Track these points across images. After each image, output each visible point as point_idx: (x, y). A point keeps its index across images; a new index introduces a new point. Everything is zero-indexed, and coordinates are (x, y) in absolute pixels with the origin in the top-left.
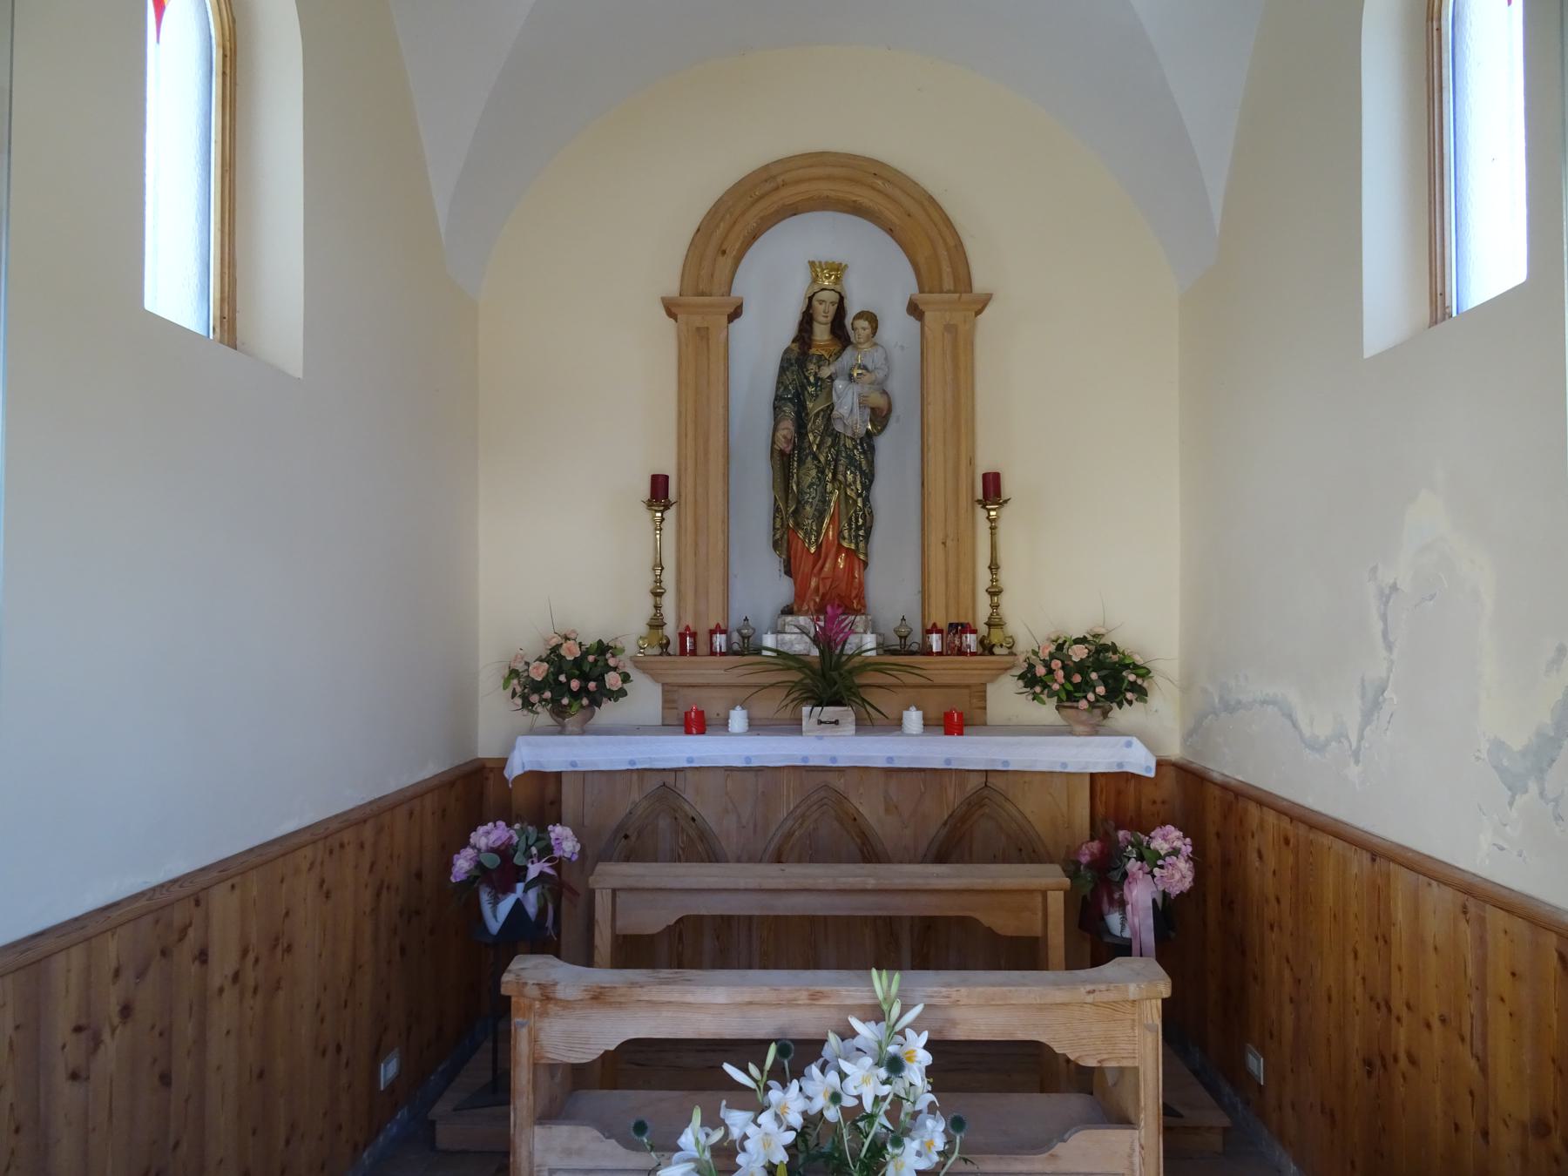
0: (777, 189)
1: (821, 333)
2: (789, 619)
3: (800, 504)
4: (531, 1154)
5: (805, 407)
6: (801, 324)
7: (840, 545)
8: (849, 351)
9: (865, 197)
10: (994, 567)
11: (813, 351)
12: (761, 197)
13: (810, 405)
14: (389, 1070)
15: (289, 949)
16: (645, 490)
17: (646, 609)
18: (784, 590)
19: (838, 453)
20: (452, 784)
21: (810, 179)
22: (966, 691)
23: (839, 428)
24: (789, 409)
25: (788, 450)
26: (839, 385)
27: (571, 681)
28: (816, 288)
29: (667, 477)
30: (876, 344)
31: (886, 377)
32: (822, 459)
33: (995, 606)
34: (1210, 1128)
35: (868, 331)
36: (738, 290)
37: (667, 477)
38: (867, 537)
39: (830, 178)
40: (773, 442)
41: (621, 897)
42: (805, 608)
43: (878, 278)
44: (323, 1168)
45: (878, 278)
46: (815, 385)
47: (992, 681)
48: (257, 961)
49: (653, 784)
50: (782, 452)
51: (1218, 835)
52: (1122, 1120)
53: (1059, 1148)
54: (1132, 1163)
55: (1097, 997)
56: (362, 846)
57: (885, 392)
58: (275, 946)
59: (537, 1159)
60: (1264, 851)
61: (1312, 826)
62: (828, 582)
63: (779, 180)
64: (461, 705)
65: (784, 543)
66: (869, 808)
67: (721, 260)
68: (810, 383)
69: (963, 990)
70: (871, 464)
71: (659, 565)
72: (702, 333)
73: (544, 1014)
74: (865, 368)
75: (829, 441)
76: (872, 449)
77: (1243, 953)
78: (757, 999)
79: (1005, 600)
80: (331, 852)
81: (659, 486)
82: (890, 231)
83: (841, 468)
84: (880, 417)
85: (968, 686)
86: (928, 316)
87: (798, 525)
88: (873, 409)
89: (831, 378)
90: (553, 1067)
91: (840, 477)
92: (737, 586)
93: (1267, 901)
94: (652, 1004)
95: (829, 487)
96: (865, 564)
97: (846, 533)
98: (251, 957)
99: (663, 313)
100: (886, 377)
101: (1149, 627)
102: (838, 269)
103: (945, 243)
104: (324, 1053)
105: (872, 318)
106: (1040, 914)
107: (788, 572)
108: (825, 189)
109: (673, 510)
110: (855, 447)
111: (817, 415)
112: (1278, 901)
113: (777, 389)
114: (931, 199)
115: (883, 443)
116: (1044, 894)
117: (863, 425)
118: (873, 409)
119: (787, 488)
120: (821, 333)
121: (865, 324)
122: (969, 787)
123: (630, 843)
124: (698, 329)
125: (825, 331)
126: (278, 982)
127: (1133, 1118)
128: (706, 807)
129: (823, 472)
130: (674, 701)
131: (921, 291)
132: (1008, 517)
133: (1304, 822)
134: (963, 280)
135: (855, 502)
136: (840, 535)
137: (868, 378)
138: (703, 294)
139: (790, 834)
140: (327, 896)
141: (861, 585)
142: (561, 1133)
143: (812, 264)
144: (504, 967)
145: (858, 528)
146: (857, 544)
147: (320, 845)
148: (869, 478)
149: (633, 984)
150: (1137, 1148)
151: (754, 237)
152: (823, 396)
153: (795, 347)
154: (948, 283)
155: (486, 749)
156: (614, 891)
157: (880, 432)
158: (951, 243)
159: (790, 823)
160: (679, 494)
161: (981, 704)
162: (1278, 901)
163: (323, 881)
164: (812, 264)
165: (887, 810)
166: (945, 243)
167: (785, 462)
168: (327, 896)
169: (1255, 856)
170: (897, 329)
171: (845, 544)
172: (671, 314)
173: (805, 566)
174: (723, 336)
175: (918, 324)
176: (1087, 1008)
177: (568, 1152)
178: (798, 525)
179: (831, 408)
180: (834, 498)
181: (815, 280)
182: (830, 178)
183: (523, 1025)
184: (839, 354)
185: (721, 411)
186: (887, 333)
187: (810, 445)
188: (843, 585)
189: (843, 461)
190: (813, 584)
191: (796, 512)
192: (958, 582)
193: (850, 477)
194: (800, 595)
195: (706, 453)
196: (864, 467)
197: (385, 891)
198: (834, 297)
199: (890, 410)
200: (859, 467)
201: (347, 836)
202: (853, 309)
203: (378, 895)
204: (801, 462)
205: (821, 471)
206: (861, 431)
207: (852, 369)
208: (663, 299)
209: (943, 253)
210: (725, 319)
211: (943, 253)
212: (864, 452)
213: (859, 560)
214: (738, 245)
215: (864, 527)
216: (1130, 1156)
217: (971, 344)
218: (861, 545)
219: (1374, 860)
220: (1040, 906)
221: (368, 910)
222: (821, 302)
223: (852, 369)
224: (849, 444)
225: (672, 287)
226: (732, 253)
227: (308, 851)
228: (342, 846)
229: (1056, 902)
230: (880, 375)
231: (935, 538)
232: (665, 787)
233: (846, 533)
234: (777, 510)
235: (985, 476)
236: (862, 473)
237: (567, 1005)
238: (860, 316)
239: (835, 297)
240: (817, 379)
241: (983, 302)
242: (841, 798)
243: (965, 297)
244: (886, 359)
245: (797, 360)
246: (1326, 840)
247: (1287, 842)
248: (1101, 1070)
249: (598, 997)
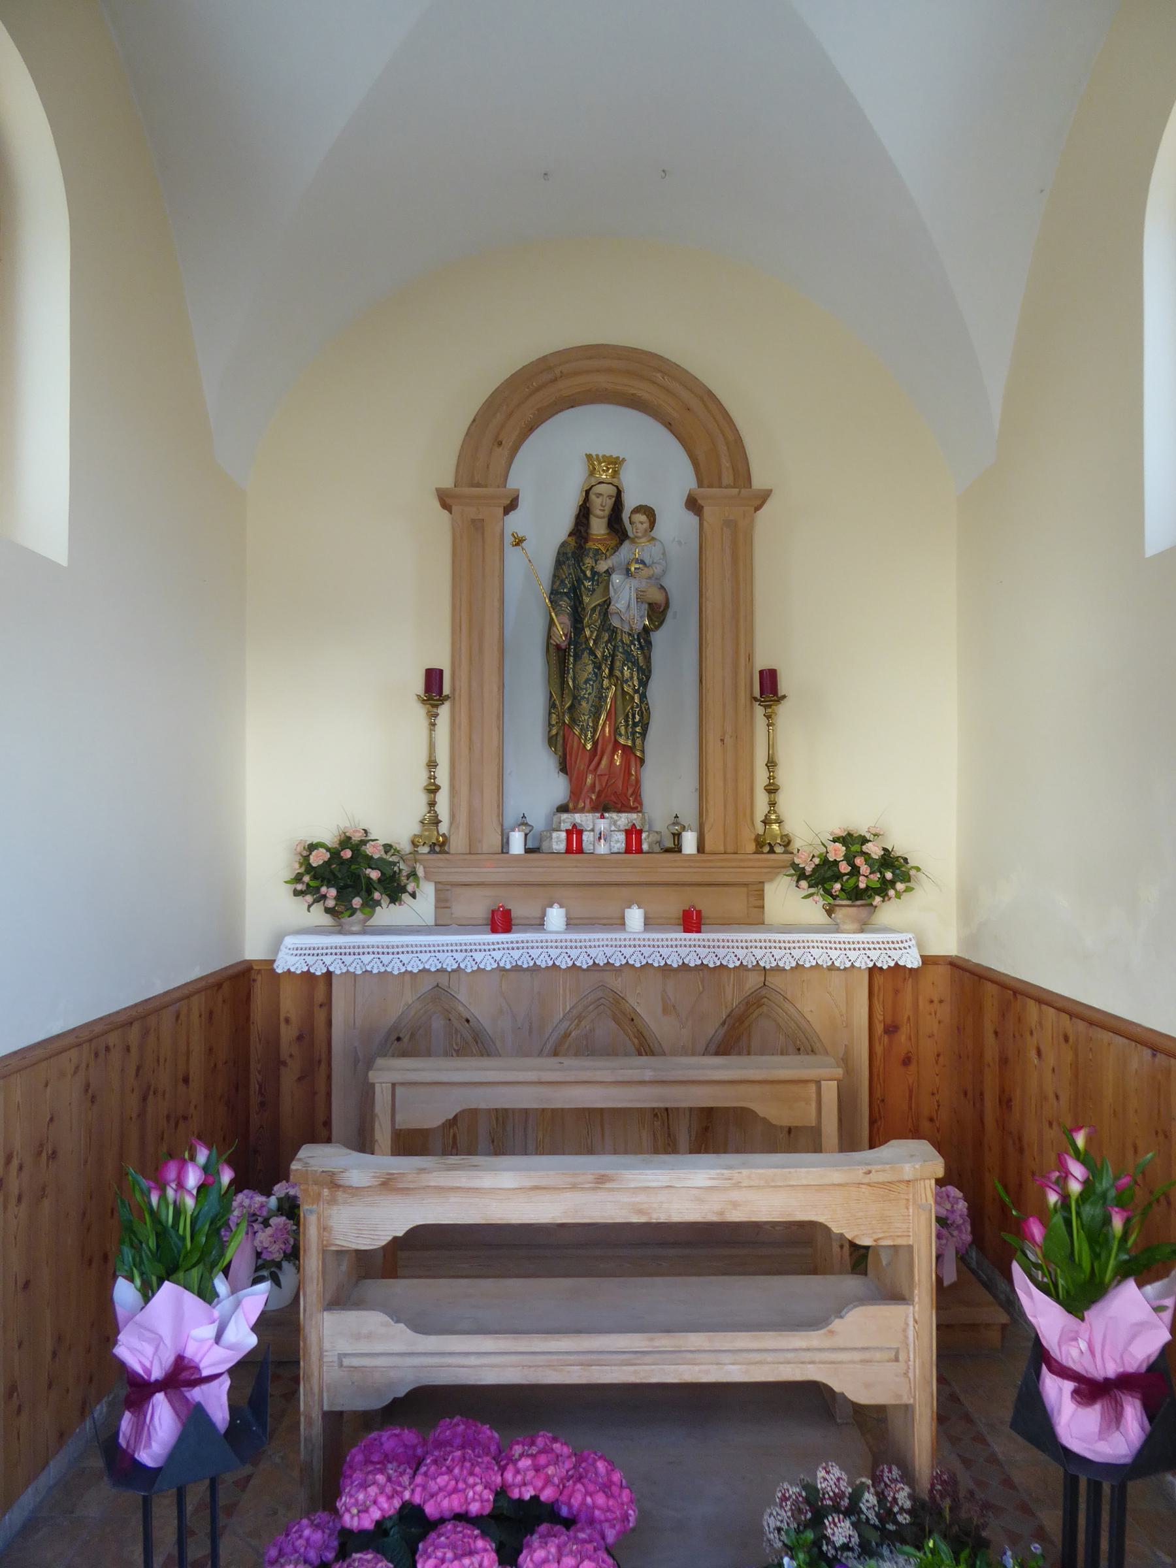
0: (555, 380)
1: (598, 527)
2: (564, 816)
4: (320, 1340)
5: (581, 602)
6: (578, 517)
7: (616, 742)
8: (627, 545)
9: (643, 390)
10: (771, 764)
11: (590, 545)
12: (538, 390)
13: (586, 600)
15: (54, 1155)
16: (419, 686)
17: (418, 805)
19: (615, 647)
20: (219, 985)
21: (588, 372)
22: (745, 889)
23: (615, 622)
24: (565, 603)
25: (564, 645)
26: (616, 579)
27: (346, 877)
29: (441, 671)
30: (653, 539)
31: (664, 572)
33: (773, 804)
34: (988, 1326)
35: (646, 525)
36: (512, 484)
37: (441, 671)
38: (644, 734)
39: (609, 370)
40: (549, 637)
41: (399, 1090)
42: (581, 805)
43: (656, 473)
44: (91, 1381)
45: (656, 473)
46: (592, 579)
47: (771, 880)
48: (21, 1168)
49: (426, 985)
50: (558, 647)
51: (996, 1033)
52: (896, 1296)
53: (837, 1324)
54: (906, 1337)
55: (874, 1177)
56: (128, 1049)
57: (662, 587)
58: (39, 1153)
59: (327, 1345)
60: (1042, 1048)
61: (1091, 1023)
63: (557, 371)
64: (226, 903)
65: (561, 743)
66: (645, 1004)
68: (586, 578)
69: (745, 1172)
70: (648, 659)
71: (432, 764)
72: (478, 526)
73: (333, 1201)
74: (643, 562)
75: (606, 636)
77: (1021, 1150)
78: (543, 1183)
79: (782, 798)
80: (96, 1055)
81: (433, 679)
82: (669, 425)
83: (618, 664)
84: (658, 612)
85: (746, 885)
86: (707, 510)
87: (574, 720)
88: (650, 604)
89: (608, 573)
90: (340, 1253)
92: (512, 784)
93: (1046, 1098)
94: (440, 1190)
95: (606, 683)
96: (642, 761)
97: (623, 730)
98: (15, 1163)
99: (437, 505)
100: (664, 572)
101: (919, 819)
102: (615, 463)
104: (90, 1262)
105: (649, 513)
106: (814, 1104)
107: (564, 768)
108: (602, 381)
110: (632, 643)
112: (1057, 1097)
113: (553, 583)
114: (710, 394)
115: (659, 638)
116: (818, 1083)
117: (639, 619)
118: (650, 604)
120: (598, 527)
121: (643, 518)
122: (748, 986)
123: (403, 1041)
124: (473, 521)
125: (603, 524)
126: (44, 1189)
127: (906, 1293)
128: (480, 1007)
129: (599, 668)
130: (447, 901)
131: (700, 484)
132: (783, 709)
133: (1083, 1019)
134: (743, 475)
136: (616, 731)
137: (645, 572)
138: (478, 485)
139: (567, 1035)
140: (93, 1100)
141: (638, 782)
142: (351, 1318)
143: (589, 457)
144: (292, 1156)
145: (635, 725)
146: (634, 741)
147: (86, 1046)
148: (645, 675)
149: (422, 1170)
150: (911, 1322)
151: (531, 429)
153: (572, 541)
154: (727, 478)
155: (253, 951)
156: (394, 1085)
157: (657, 628)
159: (566, 1024)
160: (453, 689)
161: (758, 903)
162: (1057, 1097)
163: (88, 1086)
164: (589, 457)
165: (665, 1011)
167: (560, 658)
168: (93, 1100)
169: (1033, 1054)
171: (622, 741)
172: (446, 506)
173: (581, 764)
176: (864, 1188)
177: (357, 1337)
178: (574, 720)
179: (608, 603)
180: (611, 694)
181: (592, 473)
182: (609, 370)
183: (311, 1212)
184: (616, 549)
185: (496, 604)
187: (587, 640)
189: (620, 656)
190: (589, 781)
191: (570, 708)
193: (627, 673)
194: (576, 792)
197: (151, 1097)
198: (612, 490)
199: (667, 605)
200: (635, 663)
201: (113, 1039)
202: (630, 501)
203: (145, 1099)
204: (577, 657)
206: (638, 627)
207: (629, 564)
208: (438, 490)
209: (722, 448)
210: (501, 510)
211: (722, 448)
213: (634, 757)
215: (642, 724)
216: (905, 1330)
218: (638, 742)
219: (1154, 1055)
220: (814, 1096)
221: (134, 1116)
222: (599, 495)
223: (629, 564)
224: (626, 639)
225: (447, 481)
226: (508, 444)
227: (73, 1053)
228: (107, 1049)
229: (830, 1091)
230: (657, 570)
232: (439, 988)
233: (623, 730)
234: (553, 706)
235: (761, 672)
236: (640, 669)
237: (355, 1191)
238: (638, 510)
239: (613, 491)
241: (763, 497)
242: (618, 999)
243: (743, 491)
244: (664, 553)
246: (1107, 1036)
247: (1066, 1039)
248: (876, 1249)
249: (388, 1185)
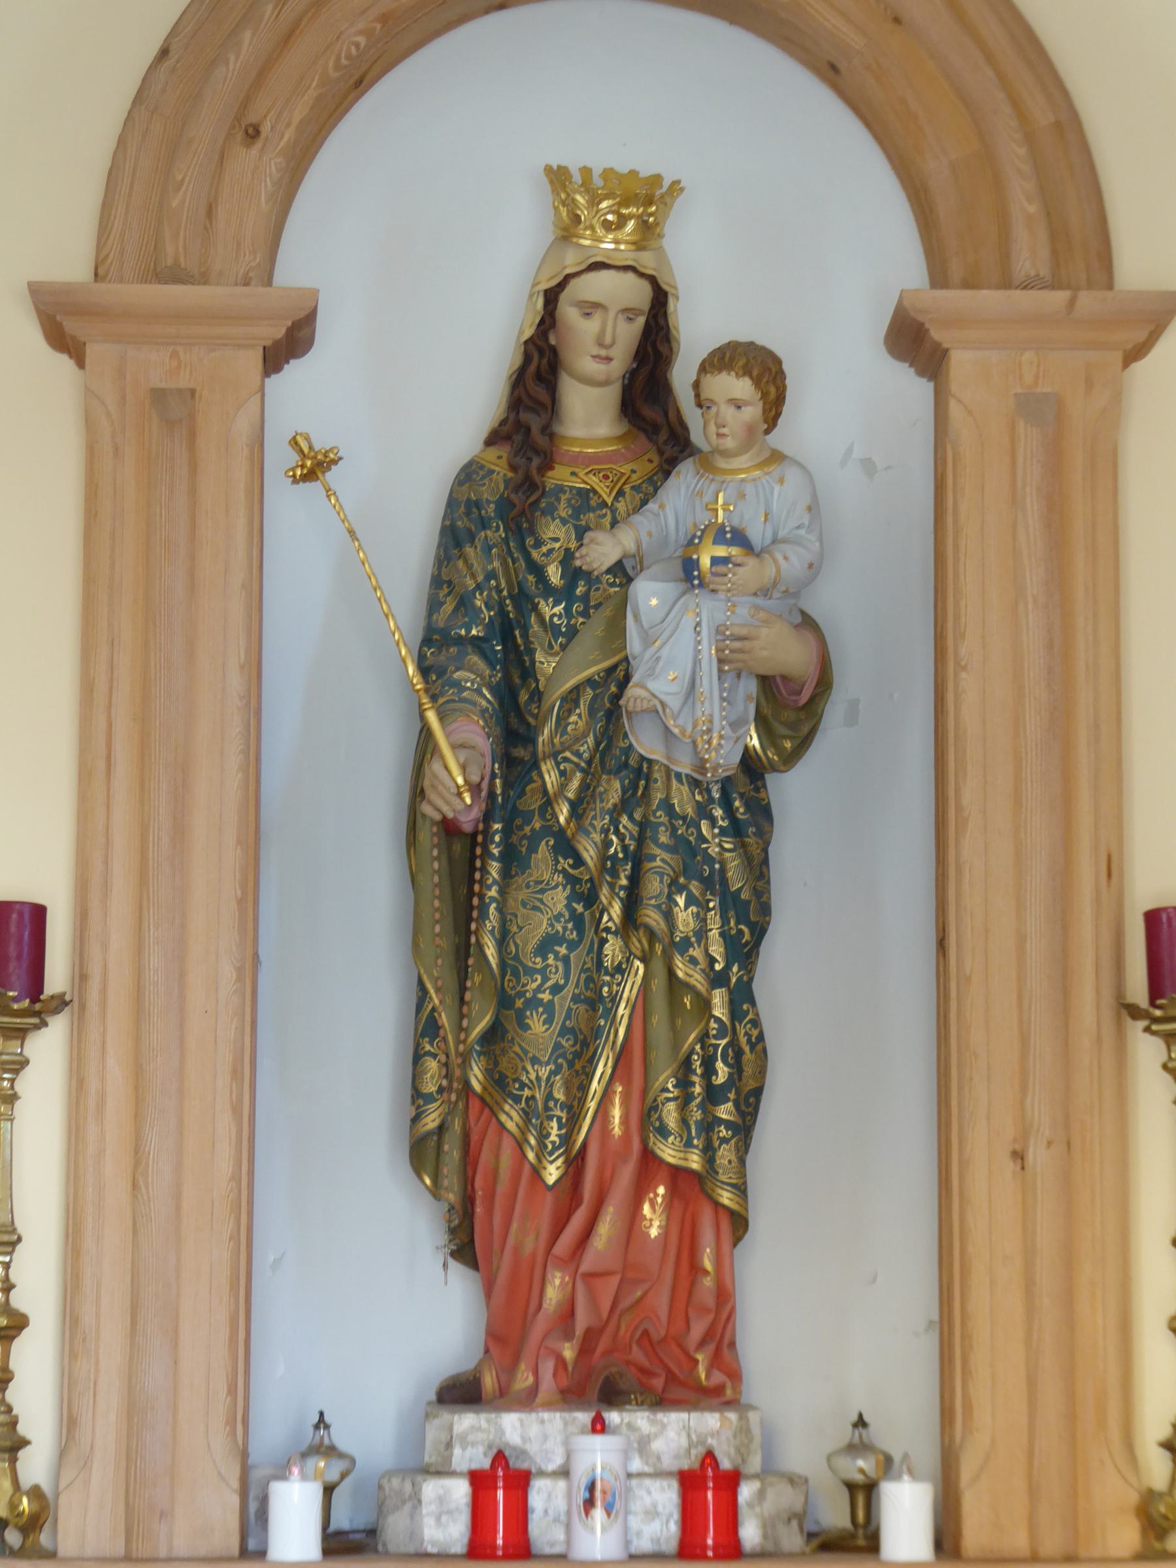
1: (588, 413)
2: (466, 1421)
3: (508, 1004)
5: (528, 672)
6: (518, 380)
7: (648, 1158)
11: (559, 475)
13: (546, 663)
14: (428, 1181)
18: (445, 1317)
23: (645, 742)
24: (474, 678)
26: (650, 595)
28: (571, 261)
30: (776, 457)
32: (589, 853)
35: (753, 412)
36: (295, 269)
37: (39, 913)
38: (744, 1129)
40: (418, 793)
42: (524, 1379)
46: (565, 594)
50: (449, 828)
57: (808, 623)
62: (607, 1290)
67: (244, 158)
68: (548, 590)
70: (759, 869)
74: (739, 538)
75: (613, 790)
76: (763, 813)
82: (831, 73)
83: (654, 886)
84: (791, 708)
87: (499, 1081)
88: (766, 682)
89: (623, 573)
91: (652, 917)
95: (613, 950)
96: (739, 1223)
97: (670, 1114)
102: (646, 201)
103: (1022, 115)
107: (465, 1247)
109: (57, 1029)
110: (703, 811)
111: (572, 699)
113: (434, 605)
118: (766, 682)
119: (464, 950)
120: (588, 413)
121: (734, 386)
124: (159, 396)
125: (606, 407)
129: (590, 899)
131: (939, 278)
133: (1022, 1103)
135: (705, 1005)
136: (647, 1118)
137: (749, 572)
138: (176, 276)
141: (724, 1296)
143: (558, 177)
145: (713, 1095)
146: (709, 1152)
152: (593, 630)
153: (498, 461)
154: (1030, 252)
157: (790, 759)
158: (1043, 115)
160: (81, 976)
166: (1022, 115)
167: (458, 866)
170: (852, 412)
171: (668, 1152)
172: (60, 338)
173: (526, 1233)
174: (243, 425)
175: (919, 390)
178: (501, 1083)
179: (620, 676)
180: (630, 989)
181: (567, 232)
185: (236, 682)
186: (810, 422)
187: (548, 803)
188: (661, 1302)
189: (661, 860)
191: (494, 1036)
192: (1068, 1298)
193: (685, 918)
194: (505, 1336)
195: (180, 830)
196: (736, 879)
199: (824, 682)
200: (715, 882)
202: (698, 329)
204: (513, 861)
205: (586, 896)
209: (1013, 154)
210: (253, 360)
211: (1013, 154)
212: (736, 829)
213: (712, 1209)
214: (299, 112)
215: (732, 1087)
217: (1106, 465)
218: (725, 1155)
222: (590, 308)
224: (683, 800)
226: (281, 135)
231: (985, 1147)
233: (670, 1114)
234: (428, 1028)
235: (1153, 919)
236: (731, 903)
238: (731, 357)
239: (637, 293)
240: (573, 574)
243: (1088, 301)
244: (813, 508)
245: (505, 506)
